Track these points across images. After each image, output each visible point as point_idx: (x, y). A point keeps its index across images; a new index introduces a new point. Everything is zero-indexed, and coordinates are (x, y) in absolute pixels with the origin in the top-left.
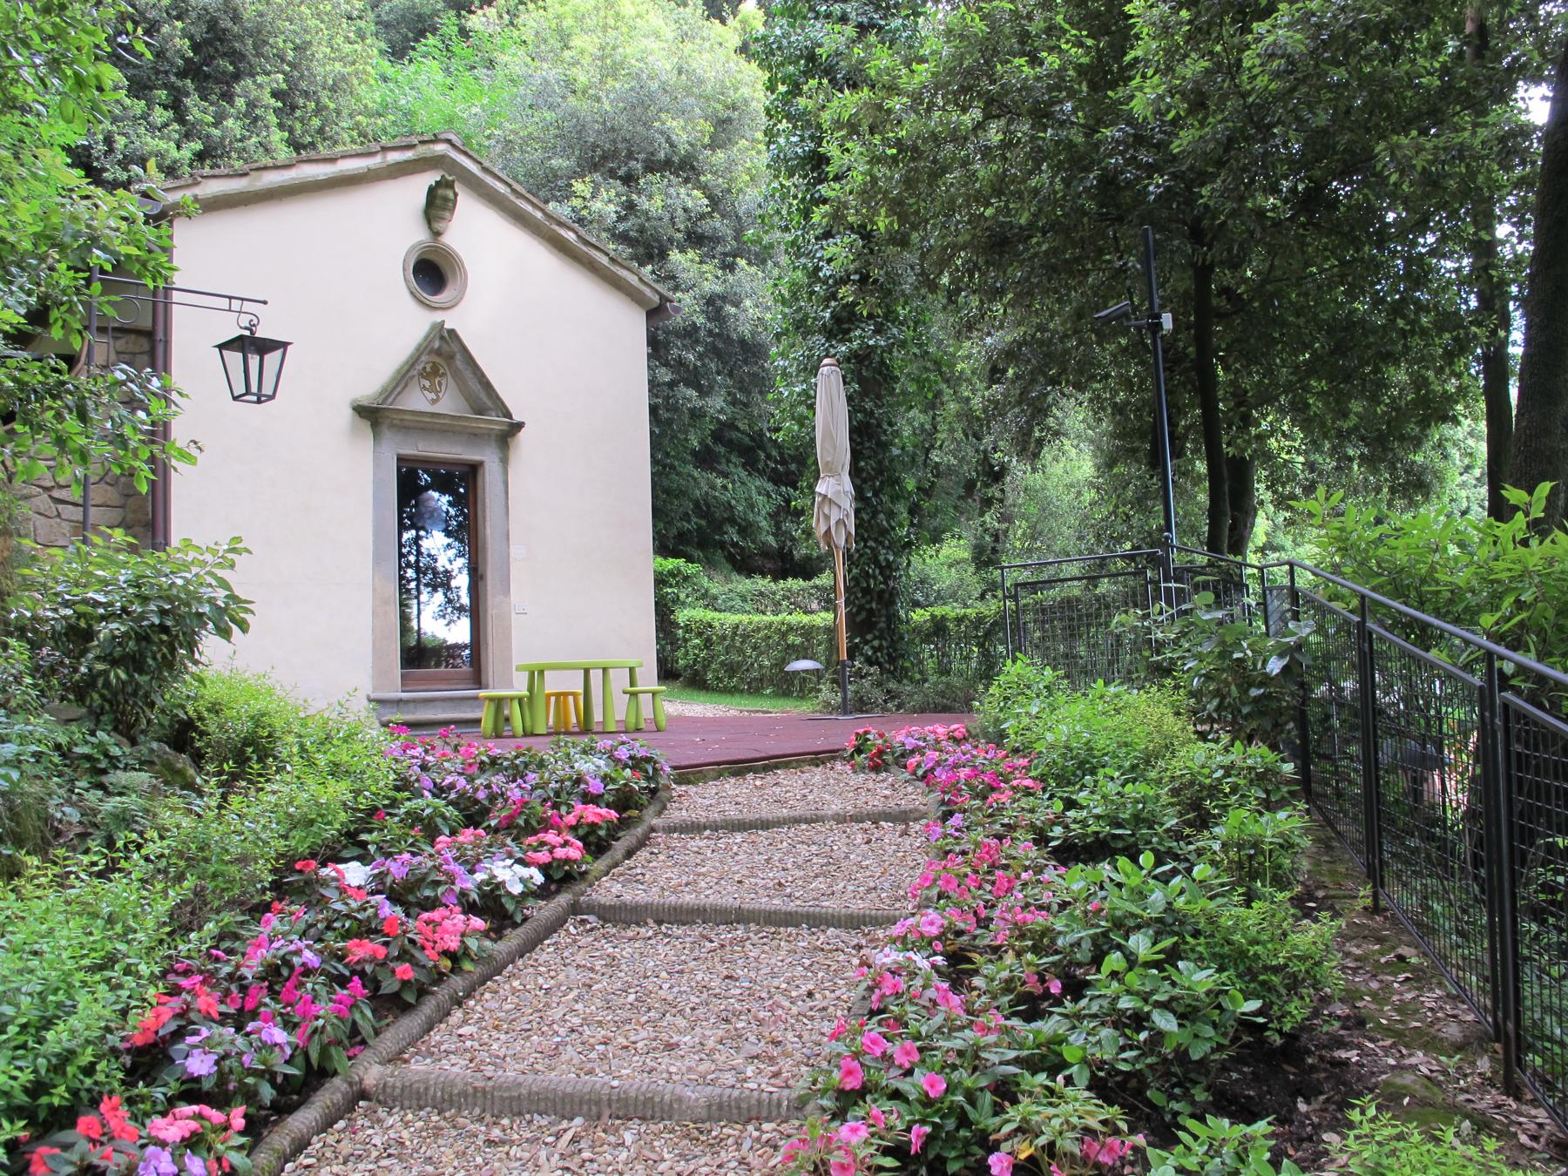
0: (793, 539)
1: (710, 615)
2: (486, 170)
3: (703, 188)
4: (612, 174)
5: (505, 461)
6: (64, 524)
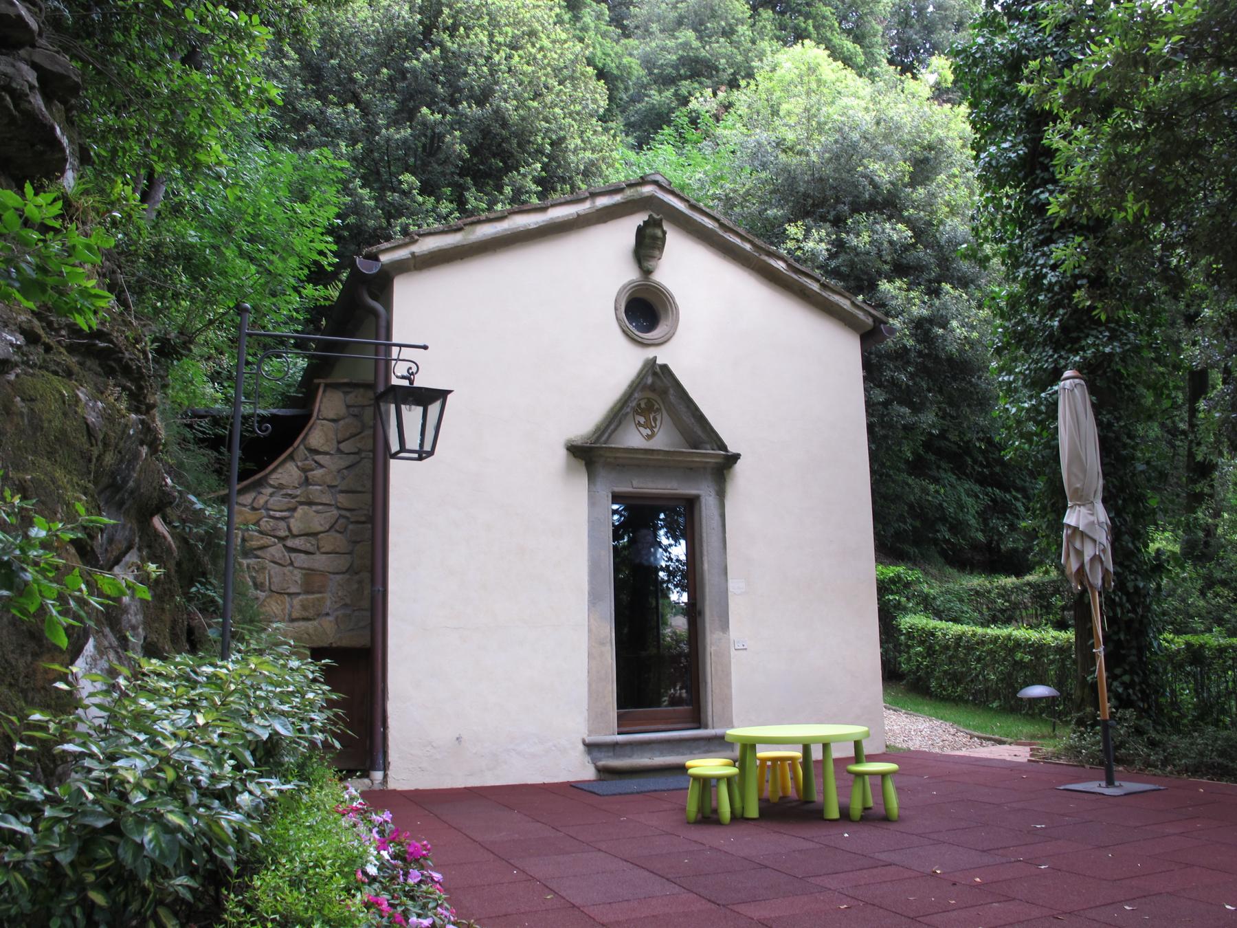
0: (1000, 534)
1: (933, 623)
2: (693, 207)
3: (908, 222)
4: (823, 219)
5: (721, 495)
6: (296, 572)
